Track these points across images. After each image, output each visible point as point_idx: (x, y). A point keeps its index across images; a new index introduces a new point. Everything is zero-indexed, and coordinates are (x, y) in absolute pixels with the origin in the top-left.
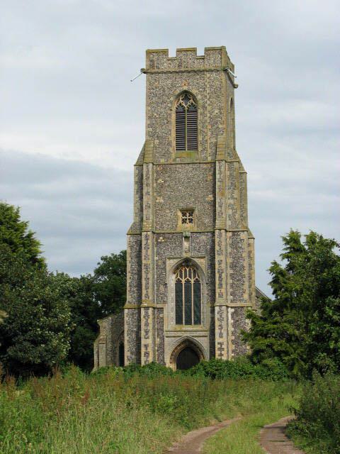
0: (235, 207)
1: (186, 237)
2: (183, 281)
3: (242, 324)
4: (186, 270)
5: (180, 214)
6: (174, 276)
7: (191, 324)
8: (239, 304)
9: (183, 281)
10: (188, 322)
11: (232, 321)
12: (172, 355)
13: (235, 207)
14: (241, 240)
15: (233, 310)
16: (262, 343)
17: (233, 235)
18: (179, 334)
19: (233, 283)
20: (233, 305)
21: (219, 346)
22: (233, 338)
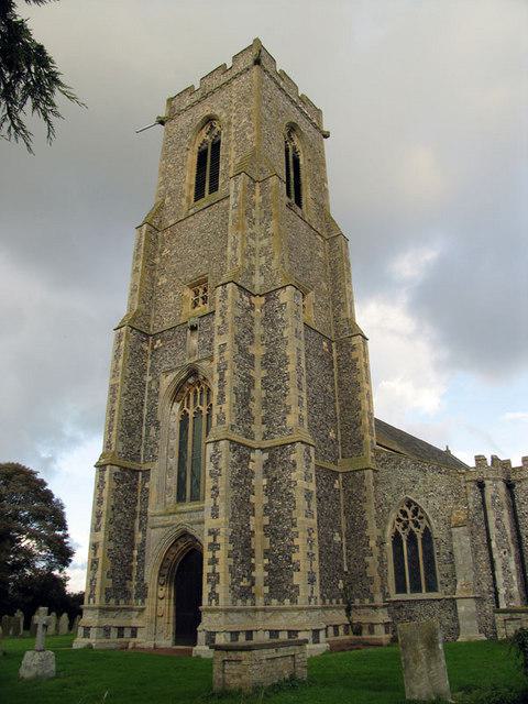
0: (271, 250)
1: (193, 328)
2: (191, 412)
3: (284, 486)
4: (196, 392)
5: (189, 293)
6: (177, 407)
7: (406, 592)
8: (278, 440)
9: (191, 412)
10: (416, 588)
11: (265, 482)
12: (162, 567)
13: (271, 250)
14: (281, 306)
15: (266, 456)
16: (495, 490)
17: (267, 300)
18: (170, 519)
19: (270, 504)
20: (267, 444)
21: (211, 539)
22: (266, 520)
